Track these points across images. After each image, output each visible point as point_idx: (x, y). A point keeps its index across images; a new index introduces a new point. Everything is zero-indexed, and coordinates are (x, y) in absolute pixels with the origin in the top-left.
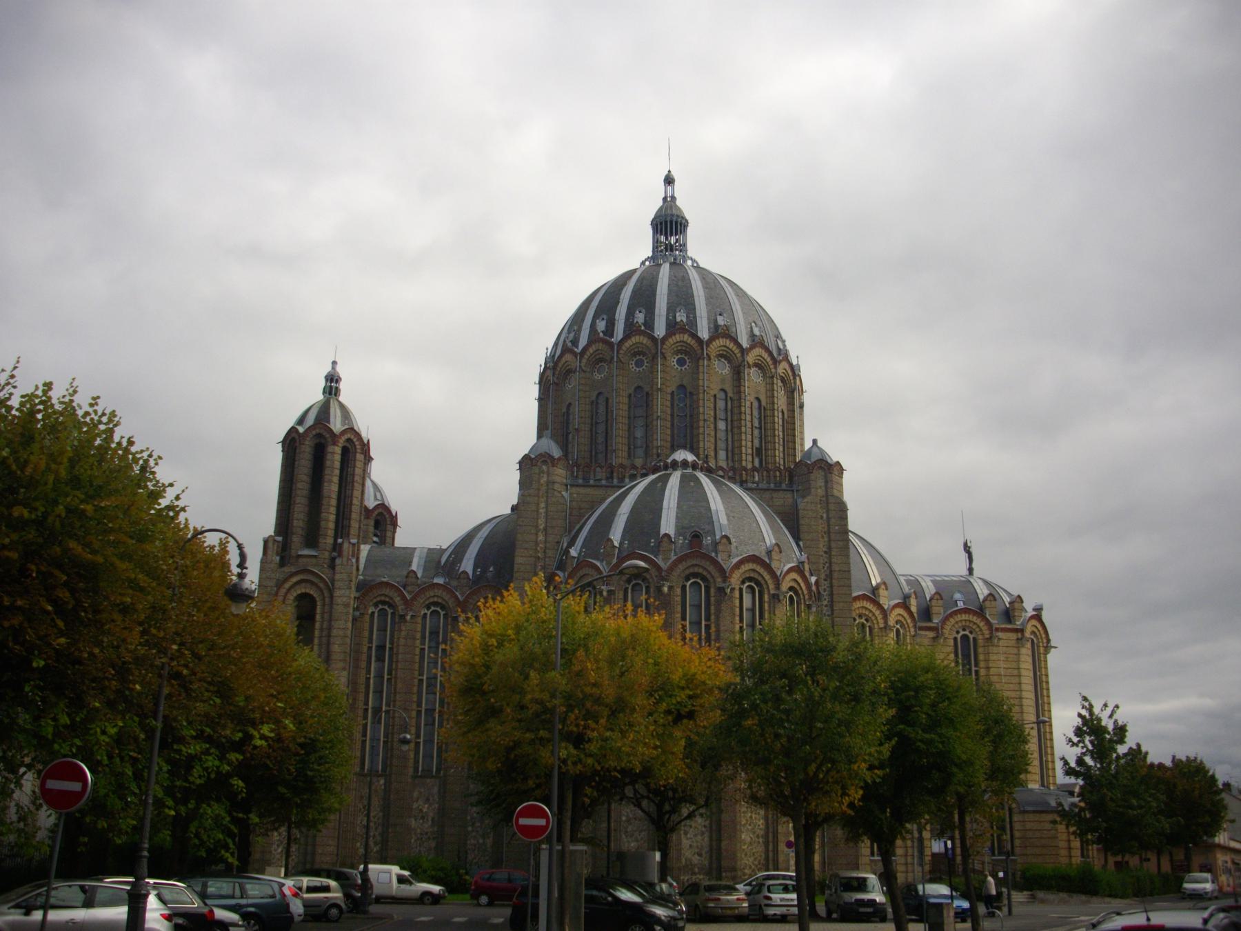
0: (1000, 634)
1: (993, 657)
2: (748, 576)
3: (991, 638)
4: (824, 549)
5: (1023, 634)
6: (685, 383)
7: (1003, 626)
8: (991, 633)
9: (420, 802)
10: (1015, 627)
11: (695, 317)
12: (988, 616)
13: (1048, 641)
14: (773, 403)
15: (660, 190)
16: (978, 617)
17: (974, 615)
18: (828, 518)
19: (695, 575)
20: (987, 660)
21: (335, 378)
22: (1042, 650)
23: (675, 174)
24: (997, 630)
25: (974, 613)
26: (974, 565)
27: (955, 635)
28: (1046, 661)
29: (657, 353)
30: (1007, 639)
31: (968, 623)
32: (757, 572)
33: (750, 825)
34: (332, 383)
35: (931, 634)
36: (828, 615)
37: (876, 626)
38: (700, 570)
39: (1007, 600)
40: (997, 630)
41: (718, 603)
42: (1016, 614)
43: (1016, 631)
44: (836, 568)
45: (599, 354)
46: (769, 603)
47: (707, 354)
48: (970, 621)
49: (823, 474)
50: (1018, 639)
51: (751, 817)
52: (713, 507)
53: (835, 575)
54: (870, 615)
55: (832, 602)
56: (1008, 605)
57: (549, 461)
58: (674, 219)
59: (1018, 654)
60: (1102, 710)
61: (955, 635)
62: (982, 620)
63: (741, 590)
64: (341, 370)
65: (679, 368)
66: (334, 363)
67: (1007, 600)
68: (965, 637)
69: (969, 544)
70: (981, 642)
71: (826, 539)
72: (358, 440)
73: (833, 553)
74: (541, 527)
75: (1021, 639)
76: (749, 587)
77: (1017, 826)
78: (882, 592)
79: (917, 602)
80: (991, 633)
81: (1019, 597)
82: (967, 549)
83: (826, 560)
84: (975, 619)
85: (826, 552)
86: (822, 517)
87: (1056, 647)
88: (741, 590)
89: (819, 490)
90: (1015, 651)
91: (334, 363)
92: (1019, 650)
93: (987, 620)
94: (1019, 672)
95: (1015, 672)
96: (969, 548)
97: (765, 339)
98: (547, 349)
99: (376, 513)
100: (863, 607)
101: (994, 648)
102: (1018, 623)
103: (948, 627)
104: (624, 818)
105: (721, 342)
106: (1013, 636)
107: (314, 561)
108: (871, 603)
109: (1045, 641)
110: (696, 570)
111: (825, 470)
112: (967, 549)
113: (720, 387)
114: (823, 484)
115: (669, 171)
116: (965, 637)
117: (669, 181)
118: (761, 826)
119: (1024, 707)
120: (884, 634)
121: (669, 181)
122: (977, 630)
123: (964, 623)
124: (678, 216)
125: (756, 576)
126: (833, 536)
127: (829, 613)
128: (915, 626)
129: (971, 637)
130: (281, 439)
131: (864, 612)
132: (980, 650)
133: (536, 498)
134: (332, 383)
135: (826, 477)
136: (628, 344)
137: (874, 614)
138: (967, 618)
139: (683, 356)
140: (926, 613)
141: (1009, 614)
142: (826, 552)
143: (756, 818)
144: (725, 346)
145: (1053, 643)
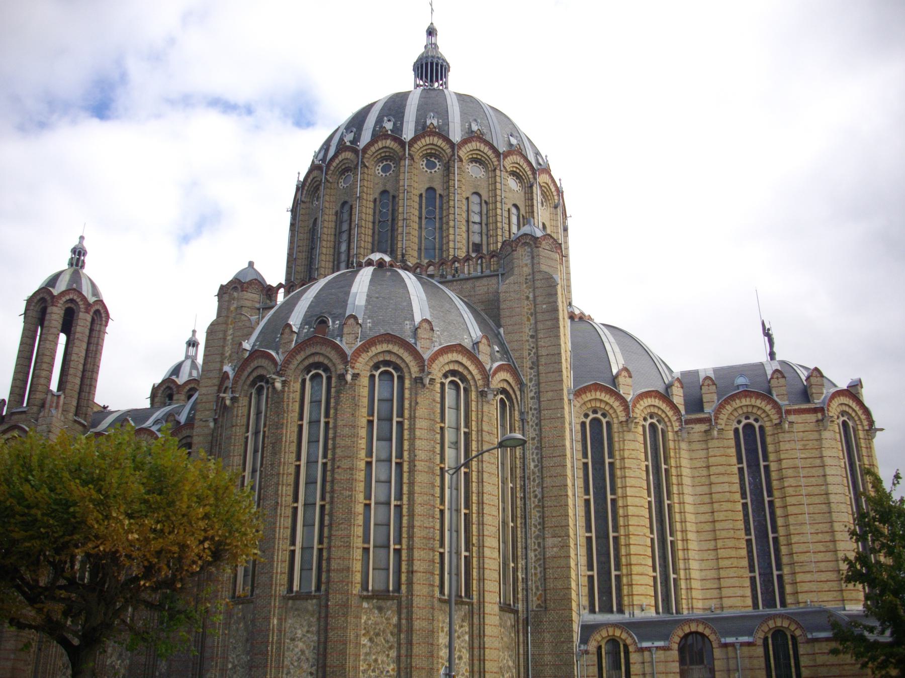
0: (792, 418)
1: (783, 446)
2: (381, 359)
3: (780, 424)
4: (530, 334)
5: (823, 414)
6: (387, 188)
7: (796, 407)
8: (781, 417)
9: (114, 658)
10: (813, 406)
11: (402, 124)
12: (775, 398)
13: (871, 423)
14: (496, 196)
15: (423, 39)
16: (763, 400)
17: (757, 398)
18: (535, 297)
19: (317, 365)
20: (777, 452)
21: (82, 252)
22: (861, 434)
23: (436, 26)
24: (788, 412)
25: (758, 395)
26: (775, 349)
27: (735, 425)
28: (870, 448)
29: (358, 163)
30: (803, 422)
31: (750, 410)
32: (395, 354)
33: (374, 671)
34: (78, 255)
35: (703, 427)
36: (535, 409)
37: (615, 421)
38: (321, 359)
39: (803, 375)
40: (788, 412)
41: (338, 392)
42: (814, 391)
43: (815, 411)
44: (543, 352)
45: (316, 182)
46: (410, 389)
47: (409, 154)
48: (753, 406)
49: (529, 250)
50: (817, 421)
51: (376, 661)
52: (354, 289)
53: (543, 361)
54: (607, 408)
55: (538, 393)
56: (805, 383)
57: (239, 287)
58: (435, 61)
59: (820, 440)
60: (894, 484)
61: (735, 425)
62: (768, 403)
63: (443, 384)
64: (86, 244)
65: (384, 175)
66: (82, 238)
67: (803, 375)
68: (749, 427)
69: (767, 326)
70: (769, 430)
71: (532, 321)
72: (82, 300)
73: (540, 335)
74: (227, 354)
75: (822, 420)
76: (452, 382)
77: (804, 661)
78: (621, 380)
79: (684, 393)
80: (781, 417)
81: (816, 369)
82: (767, 334)
83: (532, 345)
84: (758, 403)
85: (532, 337)
86: (528, 298)
87: (882, 430)
88: (443, 384)
89: (525, 269)
90: (815, 435)
91: (82, 238)
92: (820, 435)
93: (775, 403)
94: (823, 462)
95: (818, 462)
96: (769, 329)
97: (522, 147)
98: (299, 173)
99: (188, 388)
100: (596, 399)
101: (787, 435)
102: (818, 402)
103: (723, 417)
104: (230, 666)
105: (474, 145)
106: (812, 418)
107: (23, 416)
108: (606, 393)
109: (865, 423)
110: (317, 359)
111: (531, 245)
112: (767, 334)
113: (427, 186)
114: (529, 261)
115: (432, 24)
116: (749, 427)
117: (431, 32)
118: (391, 673)
119: (832, 505)
120: (625, 428)
121: (431, 32)
122: (763, 416)
123: (745, 410)
124: (438, 58)
125: (393, 359)
126: (540, 317)
127: (537, 406)
128: (680, 420)
129: (757, 425)
130: (23, 312)
131: (598, 405)
132: (769, 440)
133: (224, 326)
134: (78, 255)
135: (532, 252)
136: (420, 143)
137: (612, 407)
138: (748, 403)
139: (391, 164)
140: (695, 404)
141: (806, 394)
142: (532, 337)
143: (383, 662)
144: (433, 144)
145: (877, 425)
